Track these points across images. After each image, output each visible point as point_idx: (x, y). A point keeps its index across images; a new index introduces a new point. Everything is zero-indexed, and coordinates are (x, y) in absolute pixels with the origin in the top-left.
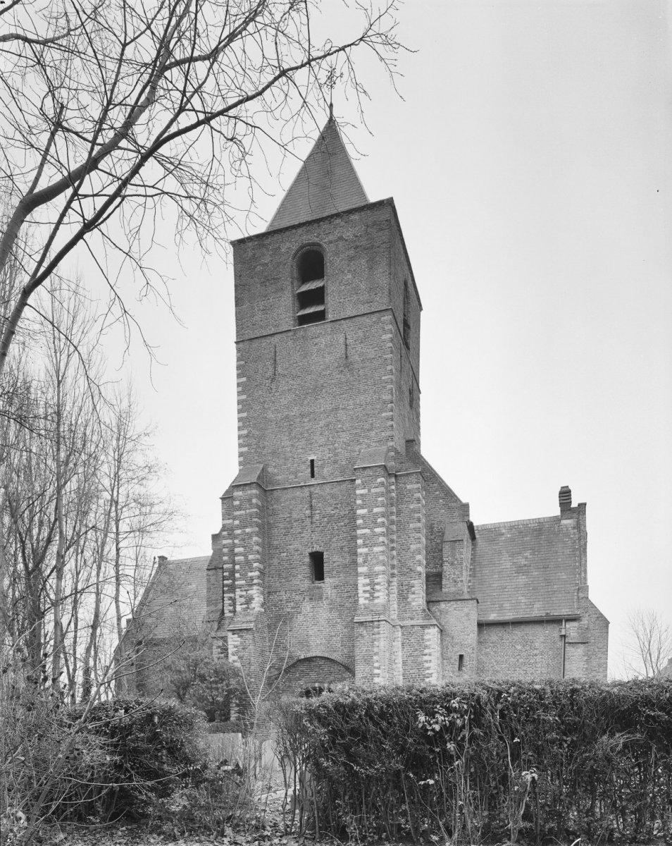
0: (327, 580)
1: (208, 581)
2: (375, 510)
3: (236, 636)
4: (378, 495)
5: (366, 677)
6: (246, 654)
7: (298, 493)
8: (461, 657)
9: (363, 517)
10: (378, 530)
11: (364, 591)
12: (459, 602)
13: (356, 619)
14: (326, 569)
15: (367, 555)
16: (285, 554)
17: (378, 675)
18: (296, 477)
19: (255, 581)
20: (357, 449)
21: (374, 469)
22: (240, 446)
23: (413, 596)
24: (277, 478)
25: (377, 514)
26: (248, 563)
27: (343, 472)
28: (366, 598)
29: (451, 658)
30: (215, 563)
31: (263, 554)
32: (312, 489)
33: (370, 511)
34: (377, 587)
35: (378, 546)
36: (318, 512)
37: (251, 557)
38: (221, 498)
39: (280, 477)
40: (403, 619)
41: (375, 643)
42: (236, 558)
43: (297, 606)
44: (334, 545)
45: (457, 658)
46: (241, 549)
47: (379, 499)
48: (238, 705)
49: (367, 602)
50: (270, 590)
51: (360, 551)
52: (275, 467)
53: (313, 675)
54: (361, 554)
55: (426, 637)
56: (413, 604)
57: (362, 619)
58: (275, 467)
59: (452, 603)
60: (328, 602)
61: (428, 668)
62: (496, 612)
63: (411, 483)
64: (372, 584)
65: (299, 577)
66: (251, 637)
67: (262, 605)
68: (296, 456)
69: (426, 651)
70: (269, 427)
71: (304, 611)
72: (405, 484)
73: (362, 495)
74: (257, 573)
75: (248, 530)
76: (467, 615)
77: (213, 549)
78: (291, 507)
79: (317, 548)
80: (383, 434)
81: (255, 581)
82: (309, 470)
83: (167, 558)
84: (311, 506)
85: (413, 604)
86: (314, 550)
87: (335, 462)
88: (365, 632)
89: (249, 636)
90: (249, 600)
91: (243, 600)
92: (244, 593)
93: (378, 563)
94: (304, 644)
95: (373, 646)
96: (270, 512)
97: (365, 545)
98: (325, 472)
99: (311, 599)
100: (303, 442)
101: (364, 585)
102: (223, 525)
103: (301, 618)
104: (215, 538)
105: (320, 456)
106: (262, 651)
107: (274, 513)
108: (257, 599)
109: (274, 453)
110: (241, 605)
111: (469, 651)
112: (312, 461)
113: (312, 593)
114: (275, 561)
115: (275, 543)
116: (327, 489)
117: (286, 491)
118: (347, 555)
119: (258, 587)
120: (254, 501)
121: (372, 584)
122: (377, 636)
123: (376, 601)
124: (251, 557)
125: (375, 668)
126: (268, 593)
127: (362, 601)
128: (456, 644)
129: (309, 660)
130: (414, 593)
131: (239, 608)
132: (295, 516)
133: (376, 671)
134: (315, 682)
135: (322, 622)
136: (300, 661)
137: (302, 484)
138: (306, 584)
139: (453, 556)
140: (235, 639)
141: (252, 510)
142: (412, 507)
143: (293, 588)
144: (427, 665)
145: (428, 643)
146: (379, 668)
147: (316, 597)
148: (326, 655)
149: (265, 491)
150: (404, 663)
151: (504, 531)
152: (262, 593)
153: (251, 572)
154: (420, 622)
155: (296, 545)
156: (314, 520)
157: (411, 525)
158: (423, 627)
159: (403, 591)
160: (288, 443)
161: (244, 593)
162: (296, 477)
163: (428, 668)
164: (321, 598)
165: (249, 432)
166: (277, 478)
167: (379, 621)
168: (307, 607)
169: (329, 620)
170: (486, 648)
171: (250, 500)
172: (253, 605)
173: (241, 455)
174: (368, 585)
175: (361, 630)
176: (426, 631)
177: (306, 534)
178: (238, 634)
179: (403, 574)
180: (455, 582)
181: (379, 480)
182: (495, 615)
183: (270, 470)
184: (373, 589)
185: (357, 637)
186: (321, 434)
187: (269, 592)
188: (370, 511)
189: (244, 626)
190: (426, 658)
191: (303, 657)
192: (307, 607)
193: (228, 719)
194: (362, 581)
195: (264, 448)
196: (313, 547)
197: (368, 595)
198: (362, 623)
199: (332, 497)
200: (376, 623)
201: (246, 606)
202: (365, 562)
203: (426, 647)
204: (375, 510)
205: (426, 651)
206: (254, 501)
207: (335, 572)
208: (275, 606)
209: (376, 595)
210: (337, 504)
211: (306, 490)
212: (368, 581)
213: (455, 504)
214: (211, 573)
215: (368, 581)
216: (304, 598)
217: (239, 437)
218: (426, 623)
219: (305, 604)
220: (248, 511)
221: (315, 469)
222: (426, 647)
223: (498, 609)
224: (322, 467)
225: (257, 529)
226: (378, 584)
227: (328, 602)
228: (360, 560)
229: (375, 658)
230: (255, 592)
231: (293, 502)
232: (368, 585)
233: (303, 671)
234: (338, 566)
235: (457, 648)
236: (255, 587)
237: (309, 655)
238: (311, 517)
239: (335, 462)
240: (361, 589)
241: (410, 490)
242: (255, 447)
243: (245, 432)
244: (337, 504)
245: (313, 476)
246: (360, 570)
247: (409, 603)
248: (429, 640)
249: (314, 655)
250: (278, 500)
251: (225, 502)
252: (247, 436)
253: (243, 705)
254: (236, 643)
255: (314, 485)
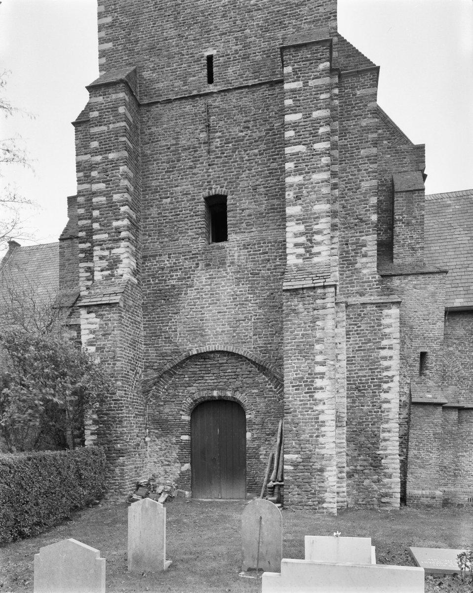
0: (231, 237)
1: (62, 254)
2: (316, 114)
3: (93, 315)
4: (319, 90)
5: (302, 378)
6: (109, 344)
7: (188, 107)
8: (423, 355)
9: (295, 126)
10: (320, 146)
11: (296, 245)
12: (420, 277)
13: (286, 285)
14: (230, 220)
15: (300, 186)
16: (169, 200)
17: (322, 375)
18: (185, 84)
19: (124, 234)
20: (279, 35)
21: (314, 48)
22: (102, 41)
23: (364, 260)
24: (157, 86)
25: (317, 121)
26: (112, 206)
27: (256, 72)
28: (299, 256)
29: (409, 357)
30: (70, 232)
31: (135, 198)
32: (210, 100)
33: (307, 116)
34: (318, 238)
35: (319, 172)
36: (219, 134)
37: (116, 197)
38: (73, 123)
39: (161, 85)
40: (348, 295)
41: (317, 323)
42: (95, 200)
43: (187, 276)
44: (242, 184)
45: (417, 356)
46: (102, 186)
47: (323, 96)
48: (95, 422)
49: (300, 261)
50: (145, 253)
51: (289, 180)
52: (154, 70)
53: (210, 380)
54: (291, 186)
55: (385, 321)
56: (365, 271)
57: (297, 285)
58: (154, 70)
59: (410, 278)
60: (233, 268)
61: (387, 368)
62: (463, 296)
63: (363, 86)
64: (309, 233)
65: (190, 234)
66: (116, 316)
67: (135, 273)
68: (184, 52)
69: (385, 343)
70: (145, 10)
71: (197, 284)
72: (353, 88)
73: (293, 91)
74: (126, 222)
75: (111, 156)
76: (433, 295)
77: (69, 216)
78: (177, 129)
79: (217, 190)
80: (321, 9)
81: (124, 234)
82: (205, 72)
83: (20, 245)
84: (208, 126)
85: (365, 271)
86: (213, 192)
87: (246, 57)
88: (301, 306)
89: (113, 315)
90: (114, 263)
91: (105, 263)
92: (106, 253)
93: (318, 200)
94: (198, 332)
95: (313, 329)
96: (146, 138)
97: (298, 171)
98: (232, 73)
99: (208, 265)
100: (196, 28)
101: (296, 235)
102: (77, 163)
103: (192, 293)
104: (71, 200)
105: (222, 50)
106: (135, 342)
107: (153, 139)
108: (125, 261)
109: (152, 49)
110: (102, 271)
111: (436, 346)
112: (210, 59)
113: (209, 255)
114: (154, 211)
115: (154, 183)
116: (233, 97)
117: (169, 106)
118: (263, 199)
119: (128, 244)
120: (122, 110)
121: (309, 233)
122: (321, 312)
123: (316, 260)
124: (116, 197)
125: (317, 363)
126: (143, 257)
127: (291, 260)
128: (417, 337)
129: (203, 356)
130: (365, 256)
131: (98, 276)
132: (183, 142)
133: (319, 369)
134: (213, 390)
135: (225, 298)
136: (190, 358)
137: (195, 93)
138: (201, 243)
139: (410, 212)
140: (91, 320)
141: (118, 125)
142: (364, 124)
143: (181, 250)
144: (385, 363)
145: (387, 331)
146: (323, 364)
147: (214, 263)
148: (230, 349)
149: (139, 105)
150: (350, 361)
151: (449, 202)
152: (135, 255)
153: (117, 220)
154: (375, 299)
155: (185, 185)
156: (213, 147)
157: (362, 151)
158: (380, 306)
159: (347, 252)
160: (173, 33)
161: (106, 253)
162: (185, 84)
163: (387, 368)
164: (223, 263)
165: (115, 21)
166: (157, 86)
167: (324, 287)
168: (201, 277)
169: (235, 296)
170: (448, 346)
171: (115, 109)
172: (120, 271)
173: (102, 54)
174: (302, 234)
175: (296, 303)
176: (386, 312)
177: (200, 170)
178: (96, 312)
179: (348, 227)
180: (413, 249)
181: (321, 66)
182: (462, 300)
183: (146, 74)
184: (310, 240)
185: (288, 315)
186: (224, 16)
187: (144, 257)
188: (307, 116)
189: (106, 300)
190: (383, 353)
191: (195, 352)
192: (201, 277)
193: (82, 443)
194: (293, 228)
195: (137, 41)
196: (211, 189)
197: (301, 251)
198: (295, 291)
199: (241, 112)
200: (319, 291)
201: (109, 272)
202: (298, 198)
203: (385, 336)
204: (316, 114)
205: (385, 343)
206: (122, 110)
207: (244, 225)
208: (154, 276)
209: (315, 250)
210: (249, 121)
211: (201, 102)
212: (301, 228)
213: (405, 147)
214: (65, 244)
215: (301, 228)
216: (197, 264)
217: (100, 28)
218: (384, 299)
219: (198, 273)
220: (111, 126)
221: (215, 69)
222: (385, 336)
223: (464, 292)
224: (226, 66)
225: (126, 154)
226: (319, 232)
227: (233, 268)
228: (290, 195)
229: (318, 347)
230: (122, 250)
231: (180, 122)
232: (302, 234)
233: (194, 373)
234: (250, 215)
235: (417, 343)
236: (123, 244)
237: (204, 349)
238: (208, 143)
239: (246, 57)
240: (291, 241)
241: (361, 98)
242: (123, 41)
243: (109, 20)
244: (249, 121)
245: (210, 80)
246: (290, 210)
247: (358, 271)
248: (389, 326)
249: (212, 348)
250: (157, 119)
251: (80, 128)
252: (111, 26)
253: (103, 422)
254: (93, 327)
255: (212, 93)
